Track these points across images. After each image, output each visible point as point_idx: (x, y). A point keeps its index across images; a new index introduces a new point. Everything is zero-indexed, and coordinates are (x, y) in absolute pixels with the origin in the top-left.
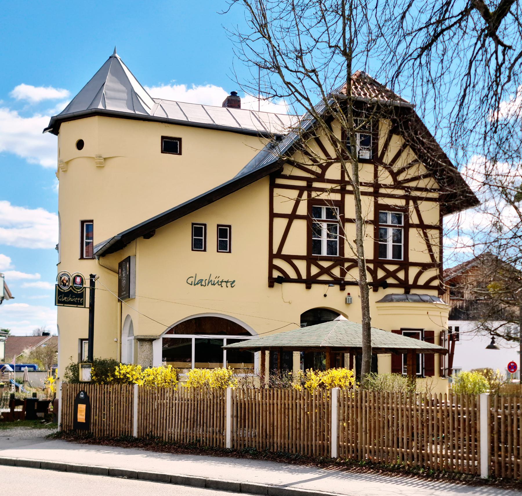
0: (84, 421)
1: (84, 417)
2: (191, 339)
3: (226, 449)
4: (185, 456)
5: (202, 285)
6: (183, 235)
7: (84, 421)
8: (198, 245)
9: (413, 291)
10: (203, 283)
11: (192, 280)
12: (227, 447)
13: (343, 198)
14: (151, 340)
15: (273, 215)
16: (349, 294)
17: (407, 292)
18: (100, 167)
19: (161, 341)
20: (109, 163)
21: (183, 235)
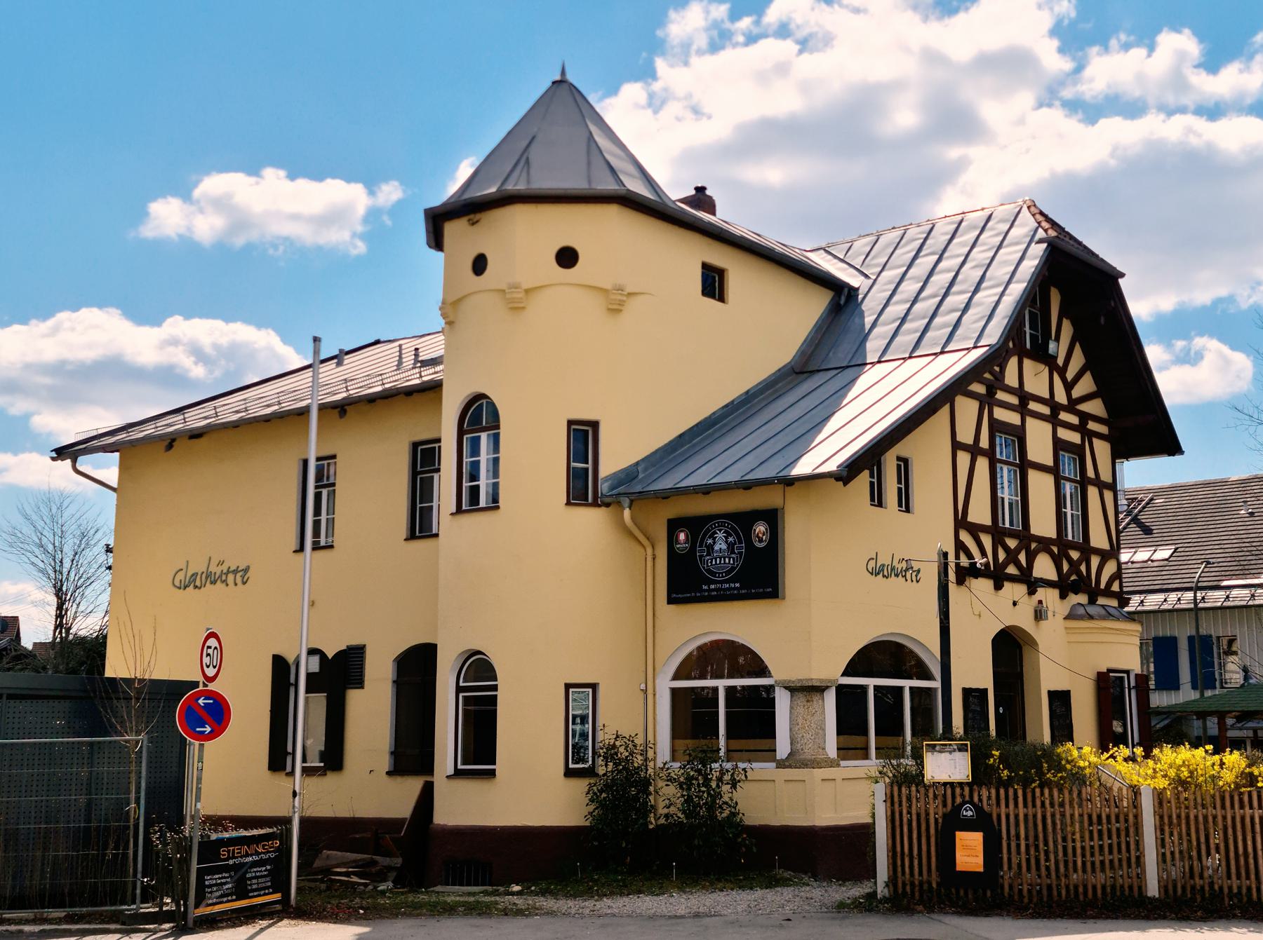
0: (981, 870)
1: (980, 860)
2: (716, 690)
3: (1153, 899)
4: (1109, 923)
5: (196, 587)
6: (272, 487)
7: (981, 870)
8: (877, 499)
9: (1101, 601)
10: (198, 583)
11: (181, 576)
12: (1150, 894)
13: (1023, 421)
14: (819, 690)
15: (956, 446)
16: (1040, 602)
17: (1092, 601)
18: (615, 310)
19: (833, 691)
20: (633, 305)
21: (272, 487)
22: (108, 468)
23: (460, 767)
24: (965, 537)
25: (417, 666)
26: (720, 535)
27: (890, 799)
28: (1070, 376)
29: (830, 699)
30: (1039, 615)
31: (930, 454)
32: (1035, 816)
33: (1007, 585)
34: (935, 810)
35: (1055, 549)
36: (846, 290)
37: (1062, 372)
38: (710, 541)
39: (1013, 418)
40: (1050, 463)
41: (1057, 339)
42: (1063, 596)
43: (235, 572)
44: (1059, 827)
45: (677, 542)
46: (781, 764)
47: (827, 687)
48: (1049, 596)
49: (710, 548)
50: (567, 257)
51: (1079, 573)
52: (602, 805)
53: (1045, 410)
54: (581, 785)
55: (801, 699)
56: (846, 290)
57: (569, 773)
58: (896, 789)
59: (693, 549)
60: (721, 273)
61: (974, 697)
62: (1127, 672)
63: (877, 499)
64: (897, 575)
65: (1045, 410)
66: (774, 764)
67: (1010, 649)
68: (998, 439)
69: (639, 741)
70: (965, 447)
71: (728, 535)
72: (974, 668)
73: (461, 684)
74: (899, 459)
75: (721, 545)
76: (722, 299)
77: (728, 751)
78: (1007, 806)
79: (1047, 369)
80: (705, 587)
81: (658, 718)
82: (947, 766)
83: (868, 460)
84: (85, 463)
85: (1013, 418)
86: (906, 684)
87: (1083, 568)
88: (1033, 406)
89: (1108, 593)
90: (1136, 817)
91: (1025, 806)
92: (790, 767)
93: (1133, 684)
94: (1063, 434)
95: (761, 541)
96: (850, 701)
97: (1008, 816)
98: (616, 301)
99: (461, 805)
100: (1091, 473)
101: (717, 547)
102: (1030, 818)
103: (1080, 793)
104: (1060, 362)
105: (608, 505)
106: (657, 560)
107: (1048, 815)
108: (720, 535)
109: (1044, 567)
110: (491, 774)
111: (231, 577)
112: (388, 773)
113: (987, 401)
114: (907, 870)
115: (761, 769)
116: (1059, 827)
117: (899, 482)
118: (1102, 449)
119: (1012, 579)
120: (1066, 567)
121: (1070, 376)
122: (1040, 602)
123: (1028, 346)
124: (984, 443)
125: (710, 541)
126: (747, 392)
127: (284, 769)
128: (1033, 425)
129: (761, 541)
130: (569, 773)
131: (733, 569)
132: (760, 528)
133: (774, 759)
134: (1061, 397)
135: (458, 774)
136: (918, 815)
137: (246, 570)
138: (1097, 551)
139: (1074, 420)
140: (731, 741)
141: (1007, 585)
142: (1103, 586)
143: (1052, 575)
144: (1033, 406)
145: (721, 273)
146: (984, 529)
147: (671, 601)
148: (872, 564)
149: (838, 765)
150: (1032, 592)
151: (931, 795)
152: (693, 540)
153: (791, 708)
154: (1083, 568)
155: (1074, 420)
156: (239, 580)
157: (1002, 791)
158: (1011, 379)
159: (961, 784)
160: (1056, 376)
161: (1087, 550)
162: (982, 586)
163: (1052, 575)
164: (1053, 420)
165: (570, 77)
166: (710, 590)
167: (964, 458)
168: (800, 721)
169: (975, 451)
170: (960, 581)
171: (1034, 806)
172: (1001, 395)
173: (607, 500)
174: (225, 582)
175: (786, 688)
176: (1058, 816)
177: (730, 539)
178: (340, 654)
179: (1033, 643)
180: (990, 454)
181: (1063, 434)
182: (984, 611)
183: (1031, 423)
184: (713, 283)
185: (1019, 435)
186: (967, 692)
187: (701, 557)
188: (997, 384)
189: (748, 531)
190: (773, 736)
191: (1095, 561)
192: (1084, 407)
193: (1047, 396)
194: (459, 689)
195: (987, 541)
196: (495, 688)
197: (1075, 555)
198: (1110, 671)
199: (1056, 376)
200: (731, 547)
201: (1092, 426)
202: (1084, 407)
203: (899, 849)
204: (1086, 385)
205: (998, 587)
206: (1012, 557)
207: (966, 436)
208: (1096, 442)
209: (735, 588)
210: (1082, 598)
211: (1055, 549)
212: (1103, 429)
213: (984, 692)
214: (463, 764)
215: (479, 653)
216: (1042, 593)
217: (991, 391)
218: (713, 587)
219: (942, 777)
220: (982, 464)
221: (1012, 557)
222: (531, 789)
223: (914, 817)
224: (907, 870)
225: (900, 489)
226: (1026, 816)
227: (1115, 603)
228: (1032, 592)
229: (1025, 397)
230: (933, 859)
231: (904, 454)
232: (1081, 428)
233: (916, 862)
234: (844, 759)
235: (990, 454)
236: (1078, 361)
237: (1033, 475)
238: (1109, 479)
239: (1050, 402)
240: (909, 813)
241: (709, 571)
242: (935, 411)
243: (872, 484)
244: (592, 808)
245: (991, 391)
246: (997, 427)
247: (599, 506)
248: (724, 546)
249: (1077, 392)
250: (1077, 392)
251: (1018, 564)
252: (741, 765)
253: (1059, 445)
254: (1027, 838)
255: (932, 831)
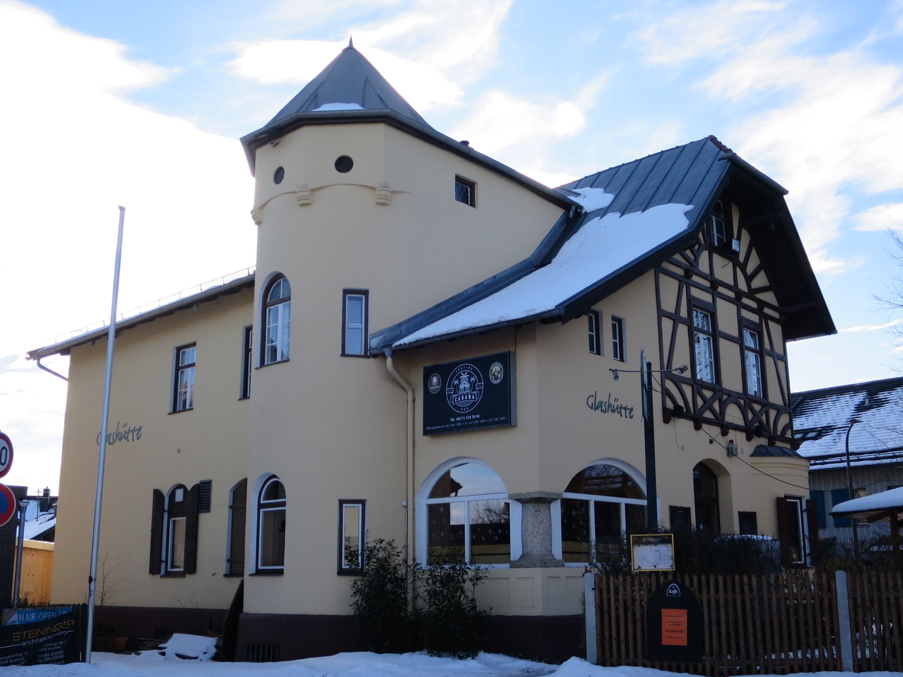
8: (596, 347)
15: (661, 314)
16: (731, 441)
17: (771, 442)
22: (62, 363)
23: (260, 567)
24: (669, 385)
25: (239, 492)
26: (464, 376)
27: (598, 589)
28: (750, 269)
29: (556, 510)
30: (731, 452)
31: (638, 311)
32: (735, 601)
33: (705, 426)
34: (641, 595)
35: (742, 402)
36: (574, 207)
37: (743, 268)
38: (456, 382)
39: (707, 297)
40: (736, 334)
41: (739, 239)
42: (749, 439)
43: (133, 431)
44: (757, 611)
45: (431, 385)
46: (514, 565)
47: (553, 500)
48: (738, 438)
49: (456, 388)
50: (344, 164)
51: (760, 421)
52: (366, 598)
53: (731, 294)
54: (348, 581)
55: (531, 508)
56: (574, 207)
57: (341, 572)
58: (604, 578)
59: (443, 389)
60: (472, 185)
61: (678, 513)
62: (800, 498)
63: (596, 347)
64: (613, 411)
65: (731, 294)
66: (508, 565)
67: (707, 476)
68: (695, 313)
69: (399, 544)
70: (668, 315)
71: (471, 375)
72: (676, 490)
73: (262, 502)
74: (614, 318)
75: (465, 385)
76: (473, 204)
77: (472, 555)
78: (708, 592)
79: (731, 264)
80: (452, 420)
81: (417, 530)
82: (653, 558)
83: (583, 306)
84: (44, 361)
85: (707, 297)
86: (623, 501)
87: (764, 418)
88: (721, 290)
89: (783, 438)
90: (830, 600)
91: (726, 591)
92: (521, 566)
93: (804, 507)
94: (745, 314)
95: (496, 378)
96: (573, 516)
97: (709, 602)
98: (385, 197)
99: (265, 598)
100: (767, 346)
101: (462, 387)
102: (730, 602)
103: (777, 578)
104: (741, 259)
105: (375, 356)
106: (417, 401)
107: (747, 599)
108: (464, 376)
109: (733, 415)
110: (280, 573)
111: (130, 434)
112: (225, 576)
113: (685, 280)
114: (615, 652)
115: (501, 568)
116: (757, 611)
117: (615, 337)
118: (776, 330)
119: (709, 422)
120: (750, 416)
121: (750, 269)
122: (731, 441)
123: (716, 244)
124: (684, 313)
125: (456, 382)
126: (494, 277)
127: (159, 572)
128: (721, 304)
129: (496, 378)
130: (341, 572)
131: (474, 403)
132: (496, 368)
133: (508, 561)
134: (743, 286)
135: (259, 573)
136: (625, 602)
137: (140, 430)
138: (774, 406)
139: (754, 305)
140: (475, 547)
141: (705, 426)
142: (779, 433)
143: (740, 422)
144: (721, 290)
145: (472, 185)
146: (686, 381)
147: (426, 433)
148: (592, 400)
149: (563, 566)
150: (724, 433)
151: (637, 582)
152: (443, 382)
153: (523, 517)
154: (764, 418)
155: (754, 305)
156: (135, 436)
157: (703, 578)
158: (703, 265)
159: (665, 573)
160: (738, 270)
161: (766, 405)
162: (684, 426)
163: (740, 422)
164: (737, 301)
165: (355, 46)
166: (456, 422)
167: (667, 324)
168: (530, 527)
169: (675, 318)
170: (666, 420)
171: (734, 591)
172: (695, 278)
173: (375, 352)
174: (127, 438)
175: (518, 500)
176: (756, 601)
177: (473, 379)
178: (196, 487)
179: (725, 473)
180: (689, 322)
181: (745, 314)
182: (683, 449)
183: (720, 302)
184: (466, 191)
185: (711, 314)
186: (674, 510)
187: (449, 395)
188: (690, 270)
189: (486, 371)
190: (508, 542)
191: (773, 413)
192: (762, 296)
193: (731, 283)
194: (260, 506)
195: (688, 390)
196: (284, 504)
197: (757, 407)
198: (787, 497)
199: (738, 270)
200: (473, 386)
201: (767, 311)
202: (762, 296)
203: (607, 633)
204: (761, 280)
205: (698, 427)
206: (708, 405)
207: (669, 305)
208: (771, 323)
209: (476, 419)
210: (763, 441)
211: (742, 402)
212: (776, 315)
213: (687, 510)
214: (263, 565)
215: (274, 476)
216: (732, 434)
217: (688, 273)
218: (458, 419)
219: (647, 567)
220: (682, 330)
221: (708, 405)
222: (311, 584)
223: (621, 603)
224: (615, 652)
225: (615, 344)
226: (726, 601)
227: (788, 446)
228: (724, 433)
229: (714, 285)
230: (639, 642)
231: (619, 314)
232: (759, 311)
233: (623, 646)
234: (567, 561)
235: (689, 322)
236: (754, 263)
237: (723, 343)
238: (781, 353)
239: (734, 288)
240: (617, 600)
241: (456, 407)
242: (641, 273)
243: (591, 337)
244: (354, 599)
245: (688, 273)
246: (693, 304)
247: (368, 357)
248: (467, 385)
249: (755, 284)
250: (755, 284)
251: (713, 411)
252: (483, 566)
253: (742, 323)
254: (727, 622)
255: (638, 617)
